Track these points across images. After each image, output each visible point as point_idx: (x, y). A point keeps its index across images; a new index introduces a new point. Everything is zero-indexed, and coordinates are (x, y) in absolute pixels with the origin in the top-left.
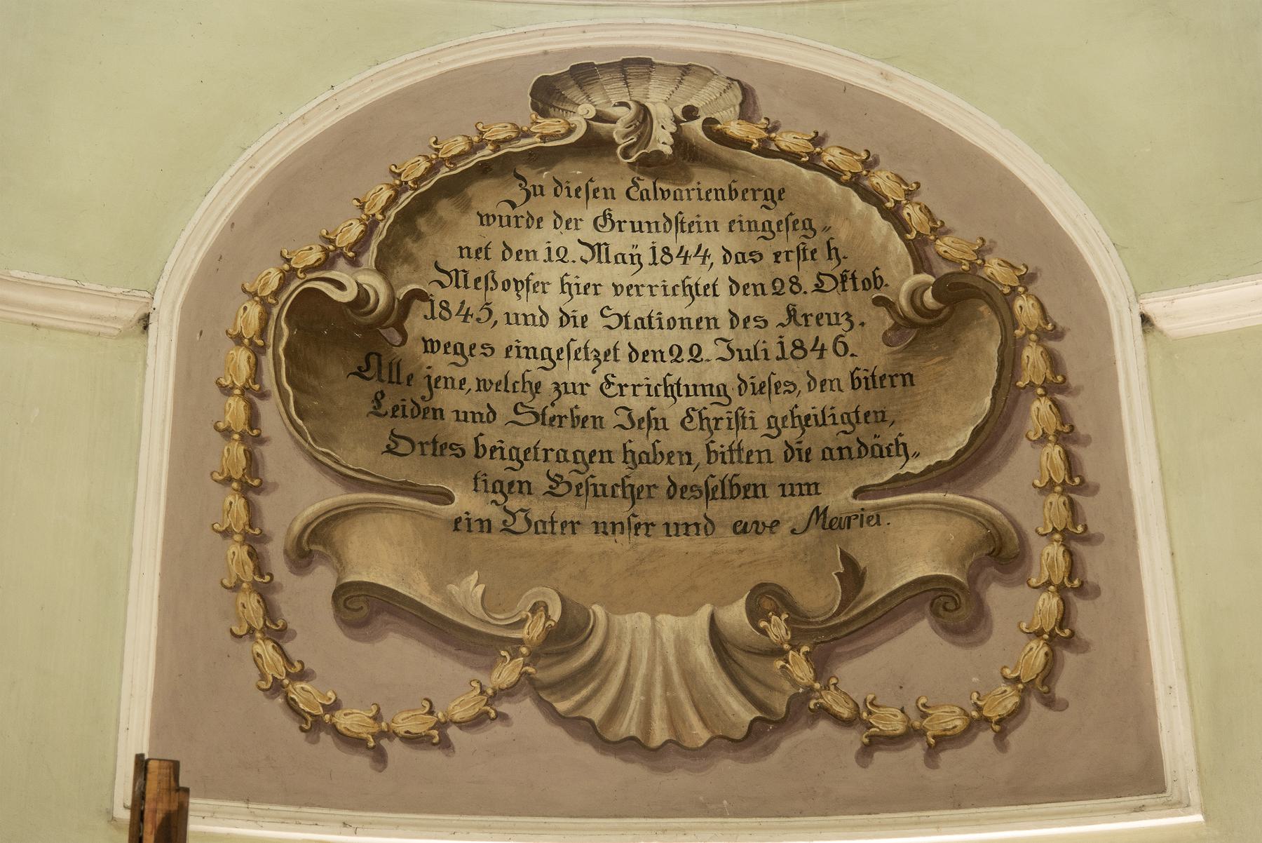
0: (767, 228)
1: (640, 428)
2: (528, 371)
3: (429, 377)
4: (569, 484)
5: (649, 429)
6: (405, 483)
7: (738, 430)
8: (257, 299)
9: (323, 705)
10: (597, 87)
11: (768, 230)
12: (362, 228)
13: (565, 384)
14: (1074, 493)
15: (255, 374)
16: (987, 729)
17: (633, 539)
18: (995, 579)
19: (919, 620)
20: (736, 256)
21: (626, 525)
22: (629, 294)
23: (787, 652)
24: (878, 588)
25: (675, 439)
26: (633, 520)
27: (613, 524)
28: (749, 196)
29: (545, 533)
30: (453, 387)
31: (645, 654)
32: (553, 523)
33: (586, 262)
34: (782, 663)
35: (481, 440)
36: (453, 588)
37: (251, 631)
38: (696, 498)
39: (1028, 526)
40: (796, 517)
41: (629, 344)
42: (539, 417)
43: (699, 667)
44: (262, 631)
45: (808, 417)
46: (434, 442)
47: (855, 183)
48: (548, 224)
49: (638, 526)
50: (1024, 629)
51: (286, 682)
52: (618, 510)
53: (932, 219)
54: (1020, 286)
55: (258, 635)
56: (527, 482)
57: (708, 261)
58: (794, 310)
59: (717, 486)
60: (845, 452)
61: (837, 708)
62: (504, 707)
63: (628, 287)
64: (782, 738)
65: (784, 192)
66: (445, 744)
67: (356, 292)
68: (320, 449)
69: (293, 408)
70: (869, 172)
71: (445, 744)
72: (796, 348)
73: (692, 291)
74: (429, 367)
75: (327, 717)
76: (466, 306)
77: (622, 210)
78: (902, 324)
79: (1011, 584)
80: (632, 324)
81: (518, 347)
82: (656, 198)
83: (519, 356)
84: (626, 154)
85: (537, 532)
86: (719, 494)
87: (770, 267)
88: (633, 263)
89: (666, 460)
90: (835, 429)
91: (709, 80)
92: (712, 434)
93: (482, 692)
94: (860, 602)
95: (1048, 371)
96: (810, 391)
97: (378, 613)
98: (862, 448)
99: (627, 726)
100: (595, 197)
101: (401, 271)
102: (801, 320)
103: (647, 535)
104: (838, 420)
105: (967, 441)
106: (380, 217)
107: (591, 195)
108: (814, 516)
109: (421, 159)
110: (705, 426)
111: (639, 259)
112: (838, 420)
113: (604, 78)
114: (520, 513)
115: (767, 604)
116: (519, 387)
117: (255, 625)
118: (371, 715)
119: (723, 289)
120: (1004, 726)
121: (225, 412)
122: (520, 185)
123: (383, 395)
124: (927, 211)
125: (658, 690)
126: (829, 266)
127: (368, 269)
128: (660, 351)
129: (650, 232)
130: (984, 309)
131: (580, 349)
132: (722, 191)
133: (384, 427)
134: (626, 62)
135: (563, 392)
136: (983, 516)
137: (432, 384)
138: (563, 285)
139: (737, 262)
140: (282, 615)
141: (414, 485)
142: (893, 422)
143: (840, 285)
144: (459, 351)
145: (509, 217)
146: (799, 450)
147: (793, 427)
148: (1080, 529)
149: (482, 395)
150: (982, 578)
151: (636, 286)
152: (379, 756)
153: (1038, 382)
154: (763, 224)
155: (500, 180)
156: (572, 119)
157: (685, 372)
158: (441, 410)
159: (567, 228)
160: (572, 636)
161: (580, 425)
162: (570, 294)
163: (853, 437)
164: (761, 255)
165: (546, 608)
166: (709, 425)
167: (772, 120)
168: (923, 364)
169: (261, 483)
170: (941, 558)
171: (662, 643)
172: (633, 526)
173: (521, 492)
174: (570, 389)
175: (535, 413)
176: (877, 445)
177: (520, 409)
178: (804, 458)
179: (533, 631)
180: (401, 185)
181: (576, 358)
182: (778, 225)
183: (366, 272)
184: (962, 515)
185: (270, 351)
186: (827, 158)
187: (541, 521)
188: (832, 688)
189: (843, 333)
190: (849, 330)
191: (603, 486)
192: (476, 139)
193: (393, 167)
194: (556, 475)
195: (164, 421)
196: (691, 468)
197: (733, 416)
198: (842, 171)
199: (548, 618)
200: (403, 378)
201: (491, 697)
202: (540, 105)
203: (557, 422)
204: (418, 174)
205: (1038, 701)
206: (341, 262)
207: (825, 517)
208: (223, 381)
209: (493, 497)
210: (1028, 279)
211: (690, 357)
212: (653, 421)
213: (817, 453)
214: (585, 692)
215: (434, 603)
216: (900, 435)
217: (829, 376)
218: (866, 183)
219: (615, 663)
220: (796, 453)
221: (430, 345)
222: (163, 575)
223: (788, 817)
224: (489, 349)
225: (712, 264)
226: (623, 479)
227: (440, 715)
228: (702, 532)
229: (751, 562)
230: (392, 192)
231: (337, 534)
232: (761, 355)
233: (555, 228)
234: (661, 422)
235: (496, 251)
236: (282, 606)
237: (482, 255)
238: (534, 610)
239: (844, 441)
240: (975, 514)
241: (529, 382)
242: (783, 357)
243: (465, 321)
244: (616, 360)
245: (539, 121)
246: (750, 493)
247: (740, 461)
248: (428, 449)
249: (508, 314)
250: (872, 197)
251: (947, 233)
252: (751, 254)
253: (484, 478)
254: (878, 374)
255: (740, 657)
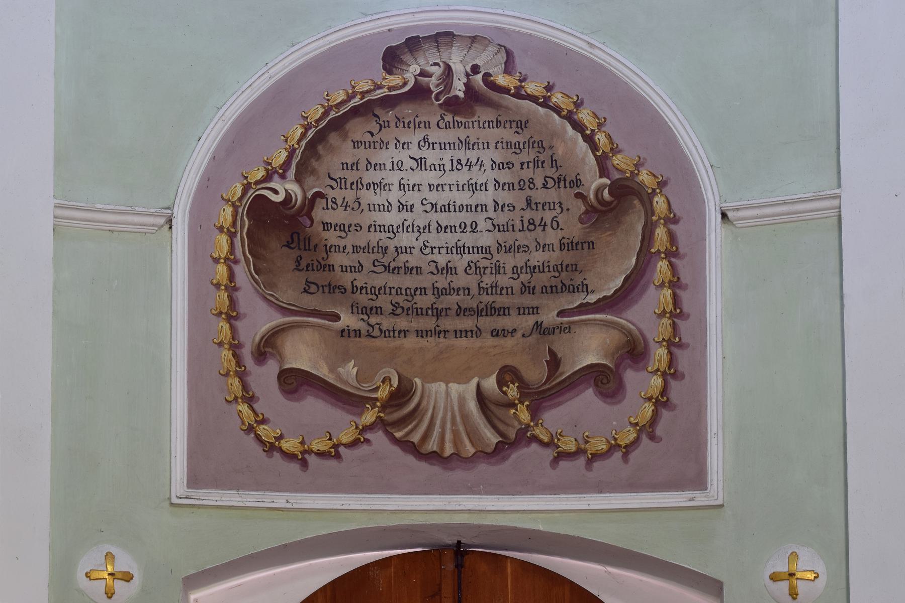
0: (517, 147)
1: (442, 273)
2: (381, 240)
3: (326, 245)
4: (403, 308)
5: (447, 274)
6: (314, 310)
7: (496, 274)
8: (230, 203)
9: (275, 437)
10: (421, 53)
11: (517, 148)
12: (286, 154)
13: (401, 247)
14: (676, 318)
15: (231, 250)
16: (619, 451)
17: (437, 339)
18: (630, 367)
19: (587, 389)
20: (499, 164)
21: (433, 332)
22: (437, 190)
23: (517, 405)
24: (568, 370)
25: (461, 280)
26: (437, 329)
27: (426, 331)
28: (508, 125)
29: (390, 337)
30: (339, 251)
31: (442, 405)
32: (394, 331)
33: (413, 170)
34: (514, 411)
35: (355, 283)
36: (341, 370)
37: (236, 398)
38: (472, 315)
39: (649, 336)
40: (525, 327)
41: (437, 222)
42: (387, 268)
43: (470, 413)
44: (241, 398)
45: (535, 267)
46: (330, 285)
47: (569, 117)
48: (392, 146)
49: (440, 332)
50: (643, 396)
51: (255, 425)
52: (428, 323)
53: (612, 142)
54: (658, 188)
55: (240, 400)
56: (380, 307)
57: (483, 168)
58: (530, 199)
59: (483, 308)
60: (554, 289)
61: (542, 437)
62: (368, 436)
63: (437, 186)
64: (512, 452)
65: (528, 122)
66: (338, 456)
67: (285, 195)
68: (268, 292)
69: (253, 269)
70: (577, 110)
71: (338, 456)
72: (530, 224)
73: (473, 187)
74: (326, 240)
75: (277, 443)
76: (346, 200)
77: (436, 136)
78: (591, 210)
79: (638, 370)
80: (438, 210)
81: (375, 225)
82: (454, 127)
83: (375, 231)
84: (437, 99)
85: (385, 337)
86: (484, 313)
87: (518, 172)
88: (440, 170)
89: (456, 293)
90: (549, 275)
91: (487, 46)
92: (482, 277)
93: (357, 428)
94: (557, 377)
95: (668, 243)
96: (537, 251)
97: (301, 385)
98: (564, 287)
99: (432, 445)
100: (419, 127)
101: (310, 180)
102: (534, 207)
103: (445, 337)
104: (551, 269)
105: (621, 284)
106: (296, 146)
107: (417, 126)
108: (535, 327)
109: (319, 106)
110: (478, 272)
111: (444, 167)
112: (551, 269)
113: (426, 46)
114: (376, 325)
115: (507, 377)
116: (376, 249)
117: (238, 395)
118: (299, 441)
119: (490, 187)
120: (628, 449)
121: (216, 273)
122: (376, 121)
123: (301, 258)
124: (609, 137)
125: (449, 426)
126: (551, 172)
127: (291, 180)
128: (454, 226)
129: (450, 149)
130: (636, 202)
131: (409, 225)
132: (492, 121)
133: (302, 277)
134: (439, 35)
135: (400, 252)
136: (625, 329)
137: (328, 250)
138: (400, 186)
139: (499, 169)
140: (251, 388)
141: (320, 311)
142: (581, 271)
143: (557, 184)
144: (342, 229)
145: (370, 142)
146: (529, 287)
147: (527, 273)
148: (677, 339)
149: (355, 255)
150: (621, 367)
151: (442, 185)
152: (304, 464)
153: (663, 250)
154: (515, 143)
155: (365, 117)
156: (407, 75)
157: (468, 239)
158: (333, 266)
159: (403, 148)
160: (404, 396)
161: (409, 272)
162: (405, 191)
163: (559, 280)
164: (513, 164)
165: (390, 380)
166: (480, 271)
167: (523, 74)
168: (600, 236)
169: (237, 314)
170: (602, 354)
171: (451, 399)
172: (437, 332)
173: (377, 313)
174: (404, 251)
175: (384, 266)
176: (572, 285)
177: (376, 264)
178: (531, 292)
179: (383, 393)
180: (308, 124)
181: (407, 231)
182: (524, 145)
183: (289, 182)
184: (614, 328)
185: (239, 235)
186: (554, 100)
187: (388, 330)
188: (540, 425)
189: (557, 215)
190: (561, 213)
191: (421, 309)
192: (350, 91)
193: (303, 113)
194: (396, 303)
195: (184, 282)
196: (470, 297)
197: (493, 266)
198: (562, 109)
199: (391, 386)
200: (312, 247)
201: (361, 430)
202: (388, 67)
203: (396, 271)
204: (318, 116)
205: (646, 436)
206: (276, 177)
207: (541, 328)
208: (214, 255)
209: (362, 316)
210: (662, 184)
211: (471, 230)
212: (450, 270)
213: (538, 290)
214: (410, 427)
215: (331, 379)
216: (585, 279)
217: (548, 242)
218: (576, 117)
219: (427, 411)
220: (527, 289)
221: (326, 226)
222: (189, 370)
223: (514, 495)
224: (359, 227)
225: (485, 170)
226: (432, 305)
227: (335, 440)
228: (474, 336)
229: (500, 353)
230: (303, 130)
231: (279, 342)
232: (510, 228)
233: (396, 148)
234: (454, 270)
235: (362, 166)
236: (251, 383)
237: (354, 168)
238: (383, 382)
239: (554, 282)
240: (622, 328)
241: (381, 246)
242: (523, 230)
243: (345, 210)
244: (429, 232)
245: (387, 77)
246: (501, 313)
247: (496, 294)
248: (326, 289)
249: (369, 204)
250: (578, 127)
251: (619, 152)
252: (507, 164)
253: (357, 305)
254: (575, 241)
255: (492, 407)
